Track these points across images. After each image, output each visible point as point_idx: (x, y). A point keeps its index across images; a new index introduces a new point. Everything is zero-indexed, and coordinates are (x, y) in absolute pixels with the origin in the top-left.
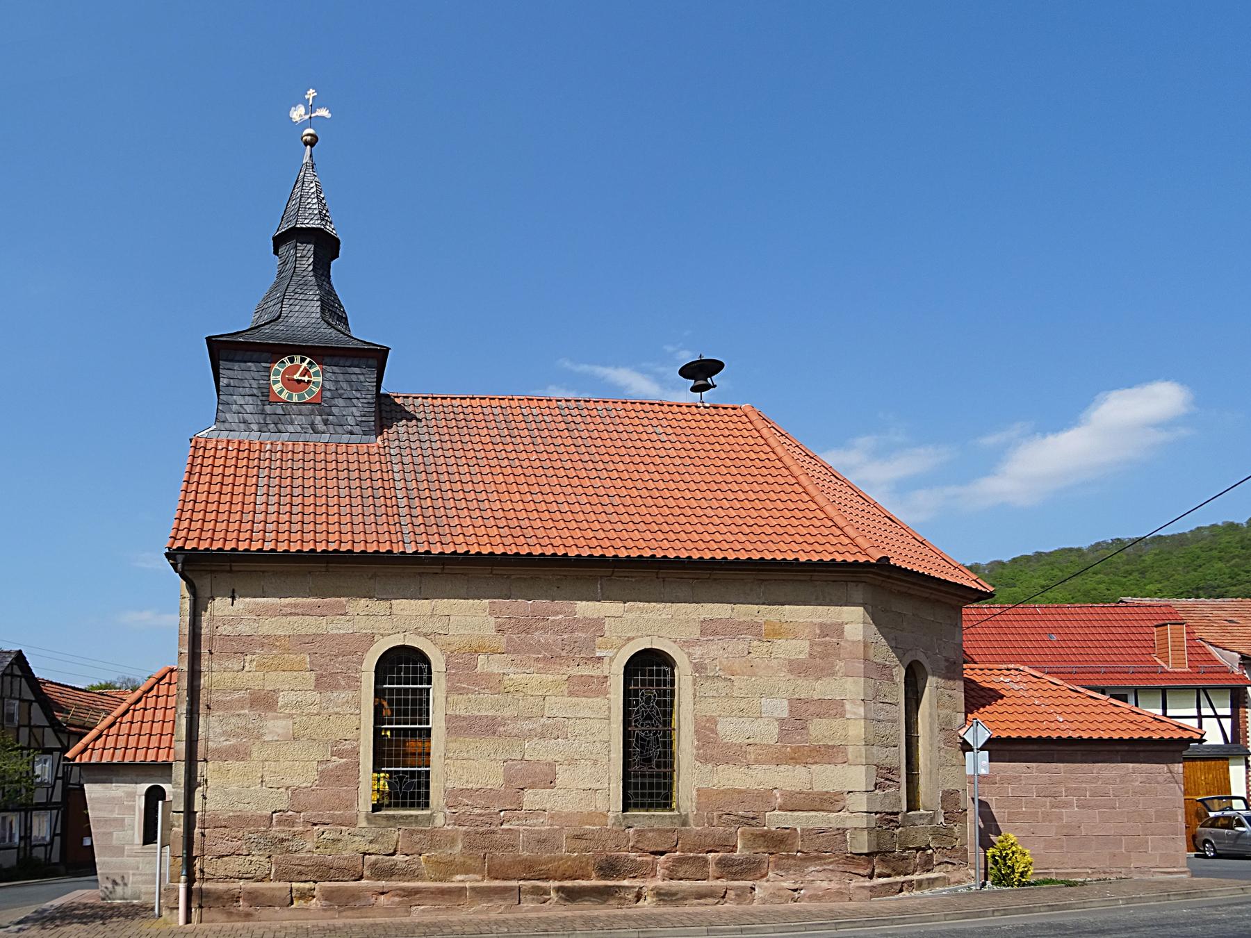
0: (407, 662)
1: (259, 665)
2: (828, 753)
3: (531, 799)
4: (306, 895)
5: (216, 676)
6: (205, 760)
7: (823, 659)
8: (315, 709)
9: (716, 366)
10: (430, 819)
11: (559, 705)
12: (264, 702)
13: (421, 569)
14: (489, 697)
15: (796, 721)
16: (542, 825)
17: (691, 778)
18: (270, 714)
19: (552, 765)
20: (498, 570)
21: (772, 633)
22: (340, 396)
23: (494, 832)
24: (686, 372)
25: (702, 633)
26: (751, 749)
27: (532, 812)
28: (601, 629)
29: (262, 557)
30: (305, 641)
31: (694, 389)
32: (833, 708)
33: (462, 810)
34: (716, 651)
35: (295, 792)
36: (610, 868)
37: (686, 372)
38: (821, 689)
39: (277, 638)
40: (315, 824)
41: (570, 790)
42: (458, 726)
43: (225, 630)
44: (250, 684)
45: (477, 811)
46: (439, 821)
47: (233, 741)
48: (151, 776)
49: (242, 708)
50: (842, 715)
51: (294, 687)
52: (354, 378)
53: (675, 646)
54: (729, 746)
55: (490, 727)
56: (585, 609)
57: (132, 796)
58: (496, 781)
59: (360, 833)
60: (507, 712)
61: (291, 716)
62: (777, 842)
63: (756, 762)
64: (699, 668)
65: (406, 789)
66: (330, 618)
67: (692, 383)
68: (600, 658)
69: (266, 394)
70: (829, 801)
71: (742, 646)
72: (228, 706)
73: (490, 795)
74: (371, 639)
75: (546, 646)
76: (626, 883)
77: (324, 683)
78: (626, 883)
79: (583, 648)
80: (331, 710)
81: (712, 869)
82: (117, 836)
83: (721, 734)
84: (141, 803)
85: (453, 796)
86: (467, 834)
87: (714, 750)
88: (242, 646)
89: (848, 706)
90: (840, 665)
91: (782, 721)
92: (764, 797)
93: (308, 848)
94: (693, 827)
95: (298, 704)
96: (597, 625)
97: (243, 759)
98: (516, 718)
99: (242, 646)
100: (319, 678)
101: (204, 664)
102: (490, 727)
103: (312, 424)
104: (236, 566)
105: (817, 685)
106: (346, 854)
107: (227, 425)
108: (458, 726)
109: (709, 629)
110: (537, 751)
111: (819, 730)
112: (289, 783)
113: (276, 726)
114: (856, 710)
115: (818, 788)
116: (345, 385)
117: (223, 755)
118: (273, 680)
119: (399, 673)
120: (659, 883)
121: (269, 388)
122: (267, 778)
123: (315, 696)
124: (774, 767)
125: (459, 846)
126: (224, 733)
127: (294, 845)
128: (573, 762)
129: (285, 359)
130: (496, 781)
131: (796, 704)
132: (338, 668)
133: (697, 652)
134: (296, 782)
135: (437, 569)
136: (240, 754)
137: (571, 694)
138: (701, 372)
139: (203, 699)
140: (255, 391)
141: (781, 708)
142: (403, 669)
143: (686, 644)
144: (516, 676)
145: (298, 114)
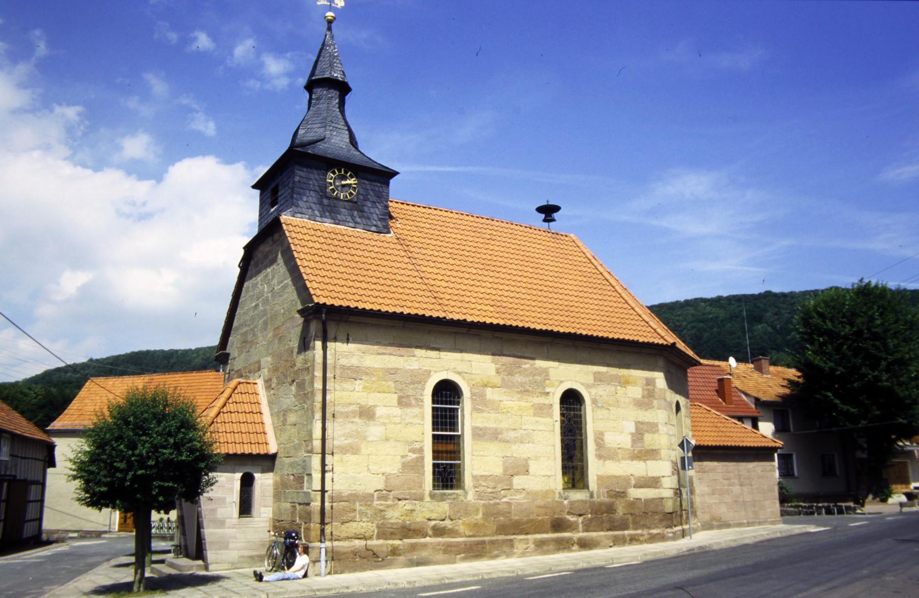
0: (446, 391)
1: (364, 388)
2: (650, 454)
3: (519, 482)
5: (338, 394)
6: (332, 454)
8: (397, 420)
9: (556, 209)
11: (530, 422)
12: (367, 413)
13: (456, 329)
14: (493, 415)
15: (638, 436)
17: (596, 468)
18: (371, 422)
19: (527, 460)
20: (497, 334)
21: (625, 383)
23: (498, 504)
24: (540, 210)
25: (595, 380)
26: (619, 451)
27: (517, 491)
28: (547, 375)
29: (364, 313)
31: (545, 221)
32: (653, 427)
33: (482, 489)
34: (602, 391)
35: (387, 477)
37: (540, 210)
38: (647, 416)
39: (376, 369)
40: (399, 500)
41: (536, 476)
42: (479, 434)
43: (343, 361)
44: (359, 401)
45: (490, 490)
47: (350, 441)
48: (245, 465)
49: (354, 417)
50: (657, 431)
51: (385, 405)
52: (377, 189)
53: (457, 376)
54: (609, 449)
55: (494, 435)
56: (540, 364)
57: (232, 480)
58: (498, 471)
60: (503, 425)
61: (384, 424)
63: (623, 458)
64: (594, 402)
65: (447, 476)
66: (406, 358)
67: (543, 216)
68: (548, 393)
70: (653, 482)
71: (613, 389)
72: (346, 415)
73: (497, 480)
74: (428, 373)
75: (522, 384)
77: (403, 402)
79: (539, 386)
80: (407, 421)
82: (221, 513)
83: (606, 442)
84: (237, 485)
86: (484, 505)
87: (605, 455)
88: (354, 373)
89: (660, 427)
90: (655, 402)
91: (632, 434)
92: (626, 480)
93: (395, 515)
95: (389, 416)
96: (546, 371)
97: (355, 454)
98: (507, 430)
99: (354, 373)
100: (400, 398)
102: (494, 435)
104: (352, 318)
105: (646, 413)
106: (418, 520)
107: (299, 209)
108: (479, 434)
109: (599, 379)
110: (521, 451)
111: (650, 440)
112: (383, 470)
113: (374, 431)
115: (650, 474)
116: (371, 193)
117: (345, 450)
118: (370, 399)
119: (442, 397)
122: (370, 467)
123: (397, 411)
124: (629, 462)
125: (480, 515)
128: (537, 458)
130: (498, 471)
132: (411, 392)
133: (593, 391)
134: (388, 470)
135: (465, 330)
136: (353, 450)
137: (535, 415)
138: (548, 211)
140: (317, 188)
142: (447, 392)
143: (588, 386)
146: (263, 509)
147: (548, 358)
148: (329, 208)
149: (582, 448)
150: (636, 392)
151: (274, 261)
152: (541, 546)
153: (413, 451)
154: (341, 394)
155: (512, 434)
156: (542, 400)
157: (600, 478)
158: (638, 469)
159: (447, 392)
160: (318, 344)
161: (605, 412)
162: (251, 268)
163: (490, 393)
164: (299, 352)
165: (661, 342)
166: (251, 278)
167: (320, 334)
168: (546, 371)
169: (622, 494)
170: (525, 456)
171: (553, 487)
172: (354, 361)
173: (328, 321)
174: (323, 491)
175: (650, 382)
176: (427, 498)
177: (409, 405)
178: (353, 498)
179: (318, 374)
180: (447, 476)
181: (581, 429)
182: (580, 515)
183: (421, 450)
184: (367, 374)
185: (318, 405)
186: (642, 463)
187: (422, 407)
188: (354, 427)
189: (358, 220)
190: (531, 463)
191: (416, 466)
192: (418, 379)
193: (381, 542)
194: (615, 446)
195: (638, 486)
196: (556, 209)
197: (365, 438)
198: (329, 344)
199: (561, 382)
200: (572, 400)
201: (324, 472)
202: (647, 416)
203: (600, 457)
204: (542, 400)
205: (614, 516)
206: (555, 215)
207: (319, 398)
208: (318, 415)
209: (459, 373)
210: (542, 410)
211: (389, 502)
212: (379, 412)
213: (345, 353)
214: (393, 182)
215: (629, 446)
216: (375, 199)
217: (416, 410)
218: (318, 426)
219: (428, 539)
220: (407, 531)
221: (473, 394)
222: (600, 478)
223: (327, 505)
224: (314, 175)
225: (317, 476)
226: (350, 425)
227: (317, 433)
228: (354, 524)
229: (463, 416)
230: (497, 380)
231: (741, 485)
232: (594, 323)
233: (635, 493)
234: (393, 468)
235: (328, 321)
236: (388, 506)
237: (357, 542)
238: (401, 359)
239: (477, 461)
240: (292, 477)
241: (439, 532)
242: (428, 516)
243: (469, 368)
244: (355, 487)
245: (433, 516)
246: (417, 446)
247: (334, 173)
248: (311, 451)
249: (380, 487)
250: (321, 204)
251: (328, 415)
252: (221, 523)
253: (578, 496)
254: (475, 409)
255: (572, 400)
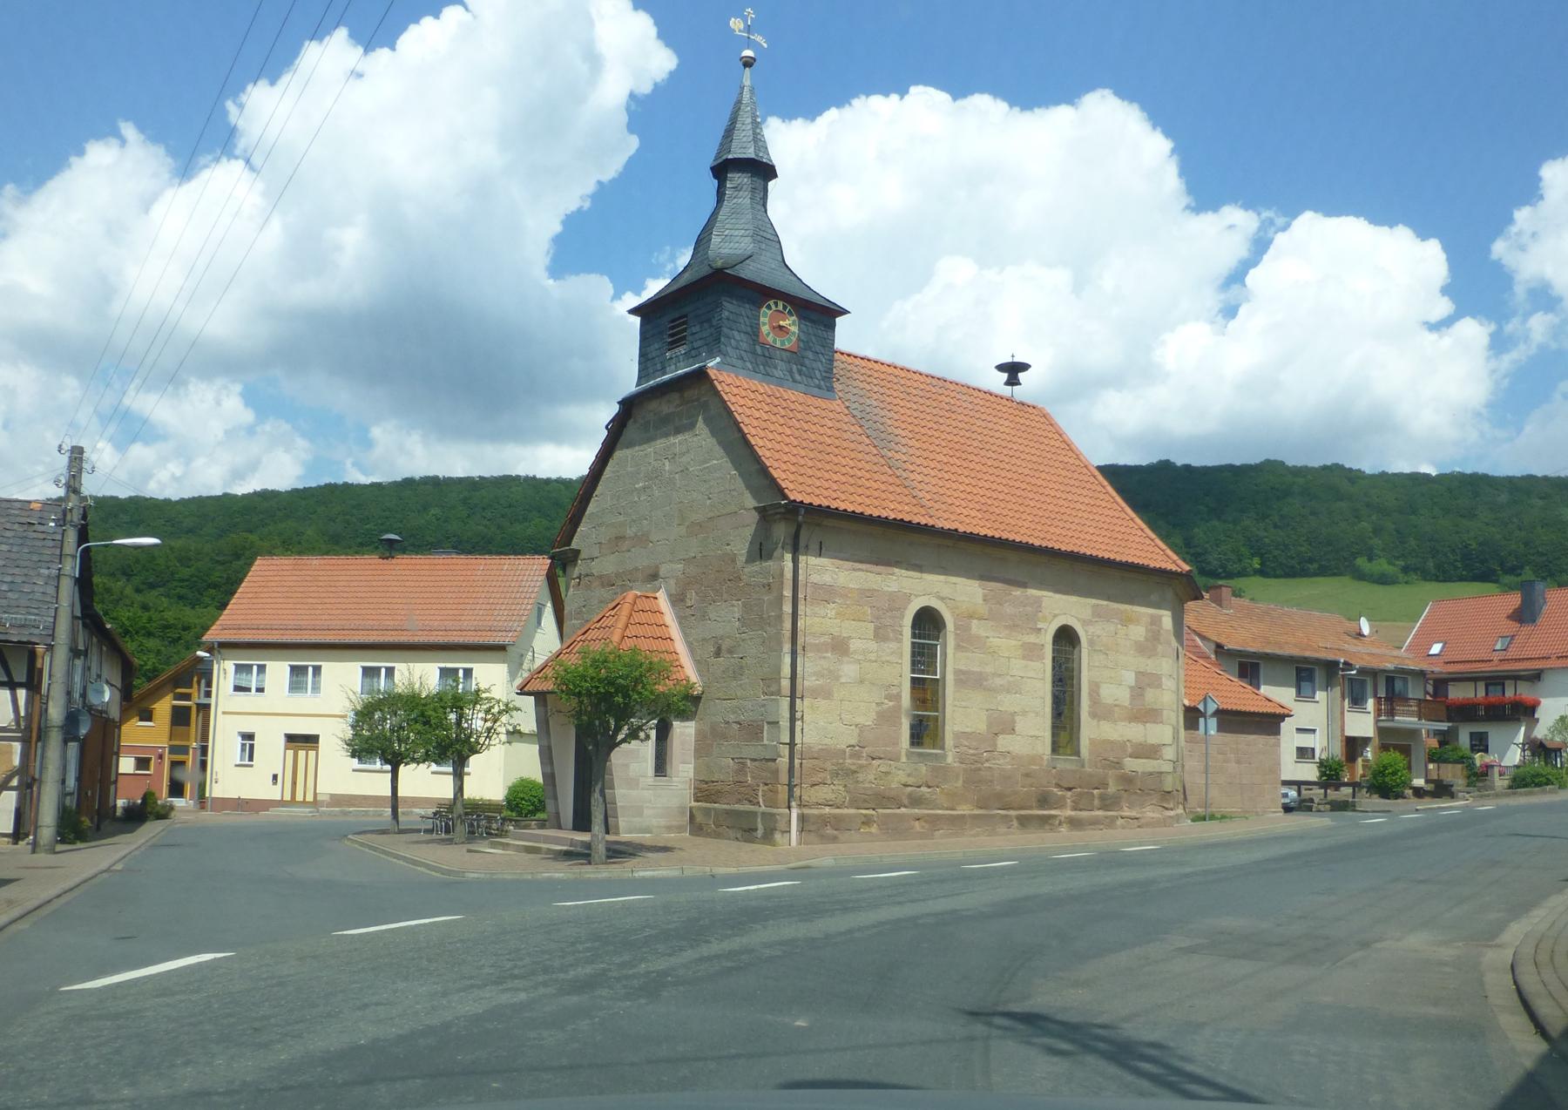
3: (1003, 742)
4: (867, 821)
7: (1147, 648)
8: (873, 657)
9: (1024, 367)
10: (944, 757)
11: (1018, 667)
12: (839, 647)
15: (1138, 691)
16: (1005, 764)
17: (1090, 730)
18: (845, 659)
21: (1127, 621)
22: (810, 349)
24: (1001, 368)
30: (867, 594)
35: (861, 728)
36: (1044, 801)
37: (1001, 368)
38: (1149, 665)
43: (815, 578)
46: (950, 760)
50: (1159, 686)
51: (861, 640)
56: (1033, 592)
58: (982, 727)
59: (902, 767)
60: (989, 669)
61: (858, 662)
62: (1128, 780)
64: (1091, 642)
65: (924, 731)
69: (755, 333)
70: (1151, 752)
71: (1112, 628)
72: (819, 648)
74: (908, 598)
76: (1053, 812)
77: (879, 636)
78: (1053, 812)
79: (1030, 624)
81: (1096, 802)
85: (959, 736)
87: (1103, 713)
88: (827, 594)
91: (1131, 687)
92: (1122, 745)
94: (1088, 769)
99: (827, 594)
100: (877, 629)
101: (801, 607)
103: (791, 372)
105: (1149, 662)
108: (964, 679)
109: (1098, 614)
110: (1008, 703)
113: (849, 670)
114: (1169, 684)
117: (816, 693)
118: (847, 628)
120: (1069, 813)
121: (758, 328)
123: (873, 645)
125: (960, 783)
126: (815, 674)
127: (861, 777)
128: (1024, 713)
129: (771, 303)
130: (982, 727)
131: (1140, 674)
133: (1091, 629)
134: (861, 720)
137: (1024, 658)
139: (800, 641)
141: (1130, 678)
142: (928, 622)
143: (1085, 623)
144: (995, 641)
145: (736, 24)
146: (681, 767)
147: (1042, 585)
148: (761, 359)
149: (1072, 702)
150: (1138, 632)
151: (692, 426)
152: (1024, 822)
153: (889, 697)
154: (817, 621)
155: (998, 681)
156: (1032, 639)
157: (1092, 742)
158: (1134, 732)
159: (928, 622)
160: (788, 557)
161: (1102, 657)
162: (631, 431)
163: (976, 627)
164: (750, 559)
165: (1174, 568)
166: (630, 445)
167: (789, 541)
168: (1038, 602)
169: (1118, 764)
170: (1011, 709)
171: (1041, 751)
172: (827, 579)
173: (793, 523)
174: (792, 744)
175: (1155, 621)
176: (904, 759)
177: (885, 639)
178: (826, 754)
179: (788, 593)
180: (924, 731)
181: (1072, 678)
182: (1070, 789)
183: (898, 697)
184: (842, 596)
185: (787, 633)
186: (1141, 727)
187: (900, 641)
188: (825, 664)
189: (798, 377)
190: (1017, 718)
191: (887, 717)
192: (895, 603)
193: (852, 811)
194: (1110, 701)
195: (1135, 756)
196: (1024, 367)
197: (837, 678)
198: (802, 558)
199: (1055, 616)
200: (1066, 638)
201: (793, 720)
202: (1149, 665)
203: (1093, 715)
204: (1032, 639)
205: (1117, 788)
206: (1021, 375)
207: (788, 625)
208: (787, 647)
209: (942, 599)
210: (1031, 652)
211: (863, 762)
212: (855, 645)
213: (820, 569)
214: (840, 321)
215: (1127, 704)
216: (818, 348)
217: (893, 645)
218: (787, 660)
219: (903, 810)
220: (883, 799)
221: (957, 627)
222: (1092, 742)
223: (797, 762)
224: (745, 310)
225: (785, 723)
226: (822, 662)
227: (786, 670)
228: (825, 789)
229: (944, 654)
230: (983, 609)
231: (1238, 762)
232: (883, 487)
233: (1133, 765)
234: (867, 719)
235: (793, 523)
236: (861, 766)
237: (827, 810)
238: (879, 578)
239: (962, 715)
240: (736, 727)
241: (916, 801)
242: (904, 779)
243: (954, 593)
244: (827, 741)
245: (910, 781)
246: (894, 691)
247: (769, 307)
248: (778, 693)
249: (853, 742)
250: (754, 353)
251: (799, 648)
252: (633, 783)
253: (1065, 763)
254: (958, 647)
255: (1066, 638)
